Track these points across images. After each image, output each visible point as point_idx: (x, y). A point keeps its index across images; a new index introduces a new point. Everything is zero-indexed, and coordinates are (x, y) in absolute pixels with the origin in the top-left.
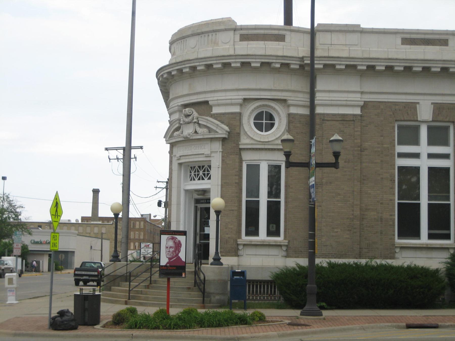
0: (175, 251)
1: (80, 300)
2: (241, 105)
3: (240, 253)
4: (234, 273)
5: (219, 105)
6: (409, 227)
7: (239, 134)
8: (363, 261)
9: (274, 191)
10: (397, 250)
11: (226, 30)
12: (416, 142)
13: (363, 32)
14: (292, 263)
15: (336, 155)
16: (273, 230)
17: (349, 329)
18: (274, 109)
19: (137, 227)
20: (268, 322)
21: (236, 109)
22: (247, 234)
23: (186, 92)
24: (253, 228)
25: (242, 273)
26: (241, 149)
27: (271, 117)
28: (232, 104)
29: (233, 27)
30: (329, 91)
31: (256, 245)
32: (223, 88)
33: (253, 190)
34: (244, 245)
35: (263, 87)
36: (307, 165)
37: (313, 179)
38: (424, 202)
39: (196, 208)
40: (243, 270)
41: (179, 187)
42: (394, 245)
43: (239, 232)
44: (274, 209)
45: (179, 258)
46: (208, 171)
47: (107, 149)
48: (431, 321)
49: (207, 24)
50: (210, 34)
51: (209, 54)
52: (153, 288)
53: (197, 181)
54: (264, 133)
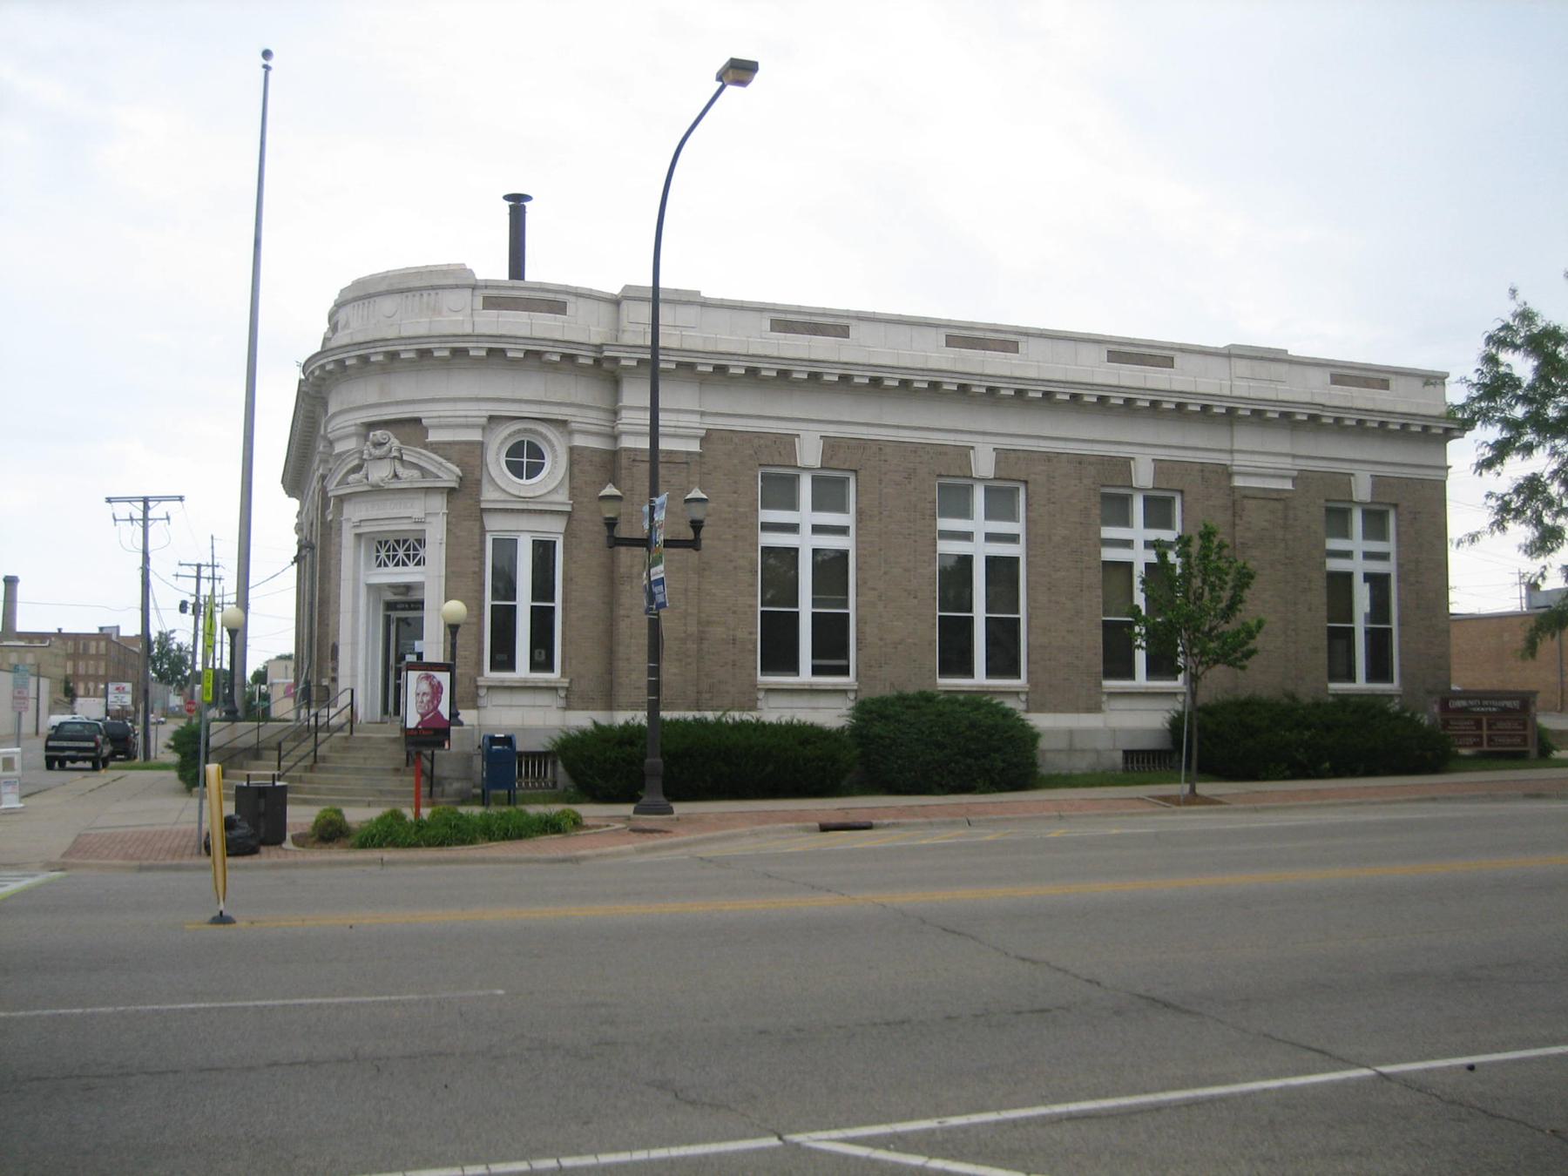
0: (431, 701)
1: (245, 796)
2: (484, 428)
3: (481, 702)
4: (494, 740)
5: (440, 427)
6: (779, 654)
7: (479, 483)
8: (710, 716)
9: (542, 587)
10: (761, 695)
11: (457, 287)
12: (793, 505)
13: (706, 304)
14: (582, 719)
15: (697, 526)
16: (542, 661)
17: (735, 836)
18: (545, 438)
19: (93, 651)
20: (588, 827)
21: (475, 436)
22: (494, 667)
23: (373, 399)
24: (502, 657)
25: (508, 741)
26: (483, 510)
27: (535, 452)
28: (467, 426)
29: (472, 282)
30: (898, 427)
31: (511, 689)
32: (451, 395)
33: (505, 587)
34: (489, 688)
35: (526, 396)
36: (646, 543)
37: (661, 567)
38: (806, 609)
39: (388, 619)
40: (509, 733)
41: (356, 580)
42: (754, 685)
43: (480, 663)
44: (542, 620)
45: (439, 715)
46: (415, 549)
47: (109, 500)
48: (852, 818)
49: (419, 273)
50: (425, 294)
51: (422, 331)
52: (322, 770)
53: (391, 568)
54: (524, 481)
